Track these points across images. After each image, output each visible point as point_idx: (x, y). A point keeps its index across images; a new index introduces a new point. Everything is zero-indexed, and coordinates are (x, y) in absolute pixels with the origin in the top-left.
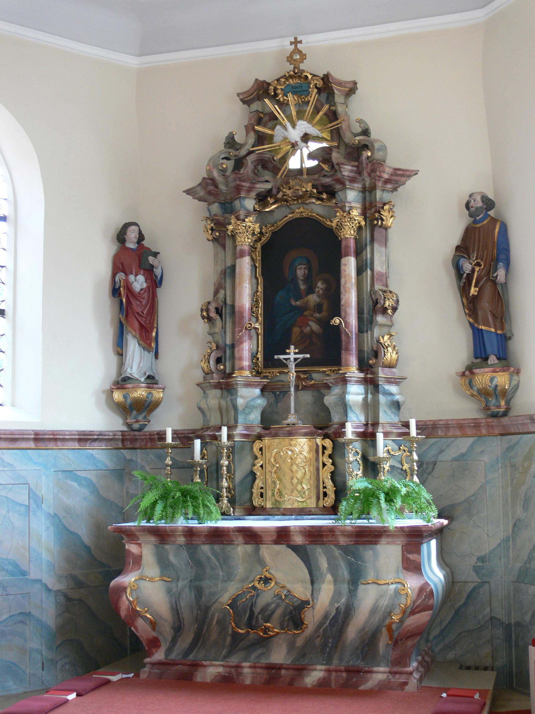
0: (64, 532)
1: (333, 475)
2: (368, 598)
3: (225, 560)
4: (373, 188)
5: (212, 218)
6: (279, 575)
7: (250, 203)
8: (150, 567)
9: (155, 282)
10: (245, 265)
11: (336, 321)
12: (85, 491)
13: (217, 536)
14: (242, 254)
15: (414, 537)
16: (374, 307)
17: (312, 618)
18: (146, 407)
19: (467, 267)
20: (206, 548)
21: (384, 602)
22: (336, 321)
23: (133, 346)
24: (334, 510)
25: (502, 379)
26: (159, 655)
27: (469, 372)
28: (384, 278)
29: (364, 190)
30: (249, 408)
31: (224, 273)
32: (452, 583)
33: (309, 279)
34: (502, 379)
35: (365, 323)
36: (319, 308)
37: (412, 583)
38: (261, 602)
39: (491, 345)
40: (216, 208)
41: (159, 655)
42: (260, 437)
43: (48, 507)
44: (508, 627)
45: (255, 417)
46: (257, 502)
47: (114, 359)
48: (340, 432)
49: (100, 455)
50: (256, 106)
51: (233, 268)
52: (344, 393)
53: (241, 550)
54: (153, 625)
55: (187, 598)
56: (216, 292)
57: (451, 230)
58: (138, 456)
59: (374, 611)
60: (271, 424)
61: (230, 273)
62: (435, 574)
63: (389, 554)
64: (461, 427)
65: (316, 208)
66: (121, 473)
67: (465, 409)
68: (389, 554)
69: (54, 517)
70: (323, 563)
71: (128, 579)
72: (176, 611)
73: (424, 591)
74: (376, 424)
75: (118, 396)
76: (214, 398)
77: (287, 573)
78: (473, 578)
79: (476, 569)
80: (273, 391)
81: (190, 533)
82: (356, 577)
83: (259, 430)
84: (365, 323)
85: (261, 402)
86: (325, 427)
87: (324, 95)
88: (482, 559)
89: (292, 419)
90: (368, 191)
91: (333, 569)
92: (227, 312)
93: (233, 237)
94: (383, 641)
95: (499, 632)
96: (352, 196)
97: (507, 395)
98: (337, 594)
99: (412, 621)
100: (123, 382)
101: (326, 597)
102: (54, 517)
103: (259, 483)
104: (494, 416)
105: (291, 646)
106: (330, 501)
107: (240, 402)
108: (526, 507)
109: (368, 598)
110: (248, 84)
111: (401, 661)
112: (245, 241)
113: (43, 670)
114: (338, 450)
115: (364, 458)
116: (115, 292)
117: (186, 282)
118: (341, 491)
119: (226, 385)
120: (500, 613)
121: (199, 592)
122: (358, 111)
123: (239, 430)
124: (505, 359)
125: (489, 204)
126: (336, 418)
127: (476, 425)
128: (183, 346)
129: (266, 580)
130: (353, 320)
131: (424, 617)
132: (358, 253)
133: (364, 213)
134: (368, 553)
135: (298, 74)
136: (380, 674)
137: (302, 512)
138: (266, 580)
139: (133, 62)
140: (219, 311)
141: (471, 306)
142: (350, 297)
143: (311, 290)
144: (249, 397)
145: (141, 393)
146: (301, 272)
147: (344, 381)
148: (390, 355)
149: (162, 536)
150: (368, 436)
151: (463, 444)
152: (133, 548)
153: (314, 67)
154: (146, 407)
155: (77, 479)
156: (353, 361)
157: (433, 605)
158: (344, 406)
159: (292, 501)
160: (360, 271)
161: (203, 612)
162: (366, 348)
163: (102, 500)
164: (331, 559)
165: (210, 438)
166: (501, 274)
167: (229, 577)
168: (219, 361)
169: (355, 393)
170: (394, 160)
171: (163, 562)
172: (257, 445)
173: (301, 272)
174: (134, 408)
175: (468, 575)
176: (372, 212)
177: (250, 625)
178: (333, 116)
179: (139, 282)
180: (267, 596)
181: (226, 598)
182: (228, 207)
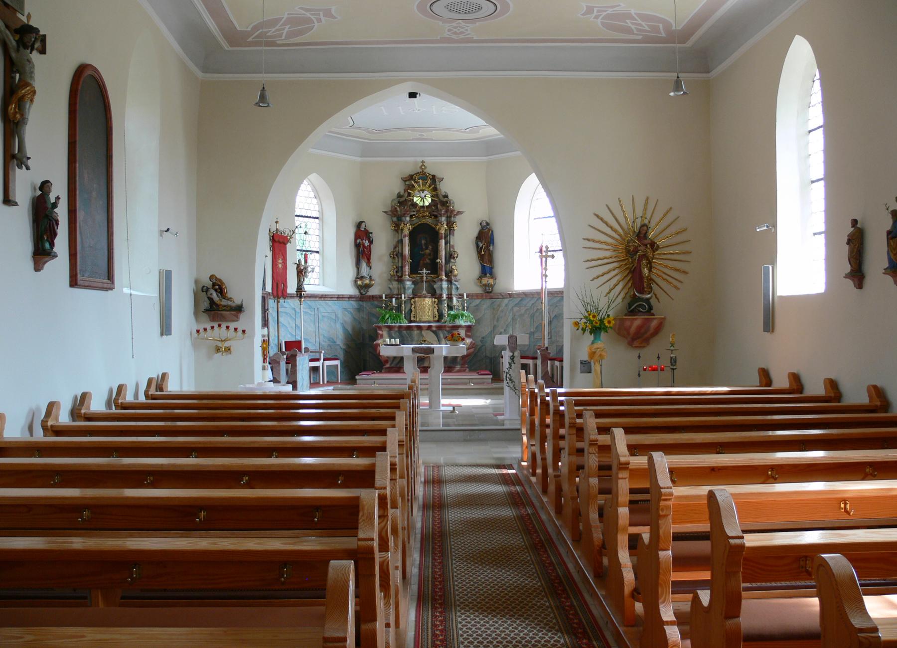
0: (345, 329)
3: (411, 336)
4: (450, 217)
7: (408, 219)
9: (371, 242)
10: (406, 240)
12: (349, 316)
14: (405, 236)
16: (450, 256)
18: (368, 286)
19: (481, 245)
23: (364, 265)
25: (491, 281)
26: (388, 365)
27: (480, 278)
28: (453, 246)
33: (426, 244)
34: (491, 281)
35: (448, 261)
36: (430, 255)
39: (487, 270)
40: (395, 219)
41: (388, 365)
44: (491, 359)
45: (410, 291)
47: (355, 269)
48: (441, 296)
50: (407, 183)
53: (416, 332)
56: (395, 248)
57: (474, 232)
58: (364, 304)
60: (416, 294)
61: (401, 242)
64: (477, 296)
65: (429, 221)
66: (359, 310)
67: (478, 290)
70: (442, 336)
75: (359, 283)
76: (395, 284)
79: (481, 341)
81: (400, 327)
84: (448, 261)
87: (432, 182)
90: (449, 218)
93: (402, 230)
95: (488, 361)
97: (492, 286)
100: (359, 277)
106: (437, 319)
108: (498, 321)
110: (406, 174)
112: (406, 232)
116: (357, 246)
117: (381, 246)
119: (400, 280)
120: (488, 355)
122: (444, 187)
124: (492, 276)
125: (488, 224)
126: (438, 292)
127: (482, 295)
128: (380, 268)
132: (445, 238)
135: (424, 174)
139: (359, 159)
140: (396, 254)
141: (481, 257)
142: (443, 253)
143: (427, 248)
145: (367, 282)
146: (423, 242)
147: (441, 280)
148: (456, 272)
149: (390, 328)
151: (478, 301)
152: (380, 332)
153: (430, 170)
158: (441, 289)
159: (426, 318)
160: (446, 244)
163: (355, 319)
165: (398, 298)
166: (491, 247)
169: (445, 285)
170: (457, 208)
173: (423, 242)
176: (450, 225)
178: (435, 189)
179: (367, 243)
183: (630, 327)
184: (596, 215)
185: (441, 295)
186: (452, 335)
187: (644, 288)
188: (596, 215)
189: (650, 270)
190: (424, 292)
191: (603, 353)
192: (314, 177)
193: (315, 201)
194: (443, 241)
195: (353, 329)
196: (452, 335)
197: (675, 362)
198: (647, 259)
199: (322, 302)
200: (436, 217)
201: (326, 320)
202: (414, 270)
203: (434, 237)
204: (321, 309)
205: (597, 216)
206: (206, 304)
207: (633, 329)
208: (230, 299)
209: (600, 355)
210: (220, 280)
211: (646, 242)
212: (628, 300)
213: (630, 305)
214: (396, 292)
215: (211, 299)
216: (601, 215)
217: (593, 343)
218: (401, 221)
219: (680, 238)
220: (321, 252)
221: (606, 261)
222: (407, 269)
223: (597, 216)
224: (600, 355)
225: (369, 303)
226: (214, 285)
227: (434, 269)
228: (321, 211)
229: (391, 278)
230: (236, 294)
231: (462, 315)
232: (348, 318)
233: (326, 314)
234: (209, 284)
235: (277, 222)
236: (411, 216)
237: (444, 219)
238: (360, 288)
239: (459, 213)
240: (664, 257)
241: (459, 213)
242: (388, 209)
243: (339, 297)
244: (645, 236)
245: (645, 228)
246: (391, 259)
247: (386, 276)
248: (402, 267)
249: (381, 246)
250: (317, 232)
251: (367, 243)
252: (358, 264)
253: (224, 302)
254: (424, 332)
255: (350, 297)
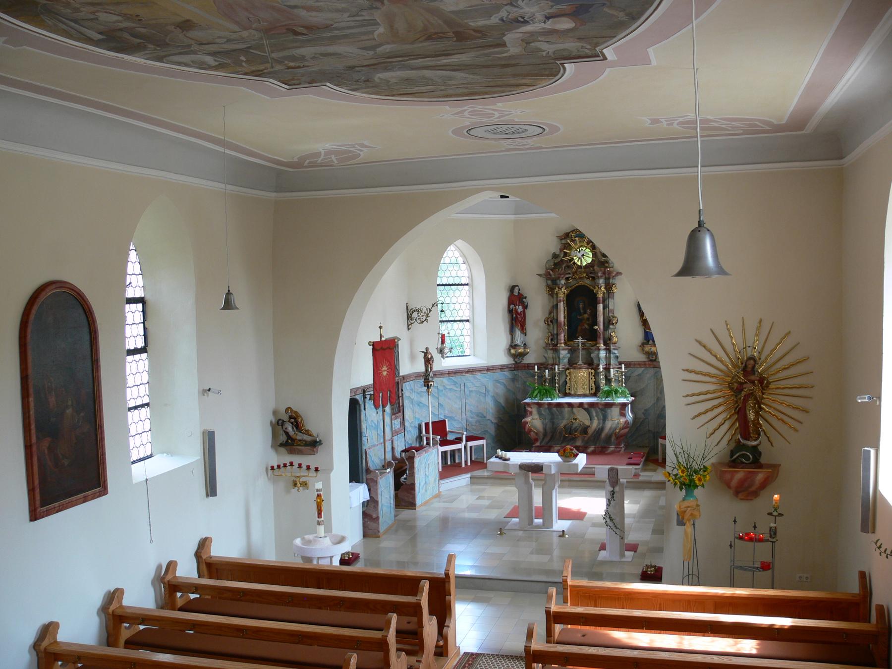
0: (496, 401)
1: (595, 382)
2: (609, 425)
3: (561, 413)
4: (609, 279)
5: (548, 286)
6: (579, 418)
7: (563, 282)
8: (535, 415)
9: (525, 307)
10: (561, 306)
11: (596, 327)
12: (502, 387)
13: (559, 405)
15: (623, 406)
16: (609, 322)
17: (590, 431)
18: (522, 355)
20: (555, 409)
21: (614, 426)
22: (596, 327)
23: (518, 333)
24: (595, 395)
25: (653, 349)
26: (538, 444)
27: (643, 345)
28: (613, 311)
29: (605, 279)
30: (564, 357)
31: (553, 307)
32: (635, 418)
33: (584, 308)
35: (606, 328)
36: (588, 319)
37: (622, 420)
38: (574, 426)
40: (549, 282)
41: (538, 444)
42: (568, 369)
43: (491, 394)
45: (566, 361)
46: (568, 391)
47: (510, 337)
49: (507, 373)
50: (563, 241)
51: (557, 305)
52: (599, 354)
53: (567, 409)
54: (537, 434)
55: (549, 425)
56: (550, 313)
58: (519, 373)
59: (611, 428)
61: (556, 307)
62: (630, 415)
63: (615, 411)
64: (639, 364)
65: (587, 282)
66: (514, 380)
68: (615, 411)
69: (493, 397)
71: (528, 419)
72: (545, 429)
73: (626, 422)
74: (610, 364)
75: (513, 351)
76: (550, 354)
77: (582, 417)
78: (643, 416)
80: (573, 351)
81: (550, 404)
82: (605, 418)
83: (567, 366)
84: (606, 328)
85: (569, 355)
86: (591, 364)
88: (646, 410)
89: (580, 363)
90: (607, 280)
91: (597, 415)
92: (554, 321)
93: (557, 294)
94: (613, 439)
96: (601, 281)
98: (599, 423)
99: (622, 431)
100: (513, 346)
101: (595, 424)
102: (493, 397)
103: (568, 385)
104: (652, 361)
105: (583, 440)
106: (593, 391)
107: (561, 356)
109: (609, 425)
110: (562, 234)
111: (619, 444)
112: (561, 296)
113: (211, 490)
114: (597, 374)
115: (606, 377)
116: (510, 311)
117: (536, 312)
118: (598, 388)
119: (555, 348)
121: (553, 423)
123: (561, 366)
126: (595, 362)
128: (535, 334)
129: (576, 419)
130: (602, 327)
131: (626, 430)
133: (605, 288)
134: (609, 411)
136: (612, 448)
137: (585, 396)
138: (576, 419)
140: (551, 321)
142: (601, 319)
143: (585, 313)
144: (564, 353)
145: (521, 350)
146: (581, 306)
147: (599, 350)
148: (615, 339)
149: (539, 405)
150: (607, 369)
151: (640, 370)
152: (529, 409)
154: (522, 355)
155: (500, 383)
156: (602, 342)
157: (559, 487)
158: (599, 358)
160: (604, 308)
161: (554, 430)
162: (606, 337)
163: (508, 390)
164: (596, 413)
167: (563, 418)
168: (552, 340)
169: (603, 354)
171: (540, 414)
172: (568, 371)
173: (581, 306)
174: (517, 353)
175: (640, 415)
176: (609, 287)
177: (570, 434)
179: (520, 309)
180: (576, 424)
181: (562, 425)
182: (554, 282)
183: (731, 479)
184: (697, 341)
185: (598, 365)
186: (564, 451)
187: (749, 434)
188: (697, 341)
189: (757, 414)
190: (580, 363)
191: (696, 513)
192: (459, 242)
193: (464, 267)
194: (601, 306)
195: (507, 400)
196: (564, 451)
197: (775, 534)
198: (756, 399)
199: (469, 376)
200: (593, 278)
201: (474, 394)
202: (571, 336)
203: (593, 300)
204: (469, 384)
205: (700, 343)
206: (283, 438)
207: (734, 483)
208: (307, 433)
209: (692, 514)
210: (296, 412)
211: (753, 378)
212: (733, 445)
213: (732, 453)
214: (551, 362)
215: (287, 433)
216: (704, 341)
217: (684, 500)
218: (556, 284)
219: (800, 369)
220: (471, 320)
221: (709, 396)
222: (562, 337)
223: (700, 343)
224: (692, 514)
225: (524, 372)
226: (291, 417)
227: (592, 336)
228: (471, 277)
229: (546, 347)
230: (312, 424)
231: (616, 392)
232: (501, 390)
233: (474, 389)
234: (285, 418)
235: (381, 327)
236: (567, 279)
237: (601, 281)
238: (514, 356)
239: (619, 274)
240: (779, 391)
241: (619, 274)
242: (543, 272)
243: (489, 369)
244: (753, 371)
245: (752, 362)
246: (546, 326)
247: (542, 343)
248: (557, 334)
249: (536, 312)
250: (467, 300)
251: (520, 309)
252: (512, 332)
253: (300, 436)
254: (575, 410)
255: (502, 367)
